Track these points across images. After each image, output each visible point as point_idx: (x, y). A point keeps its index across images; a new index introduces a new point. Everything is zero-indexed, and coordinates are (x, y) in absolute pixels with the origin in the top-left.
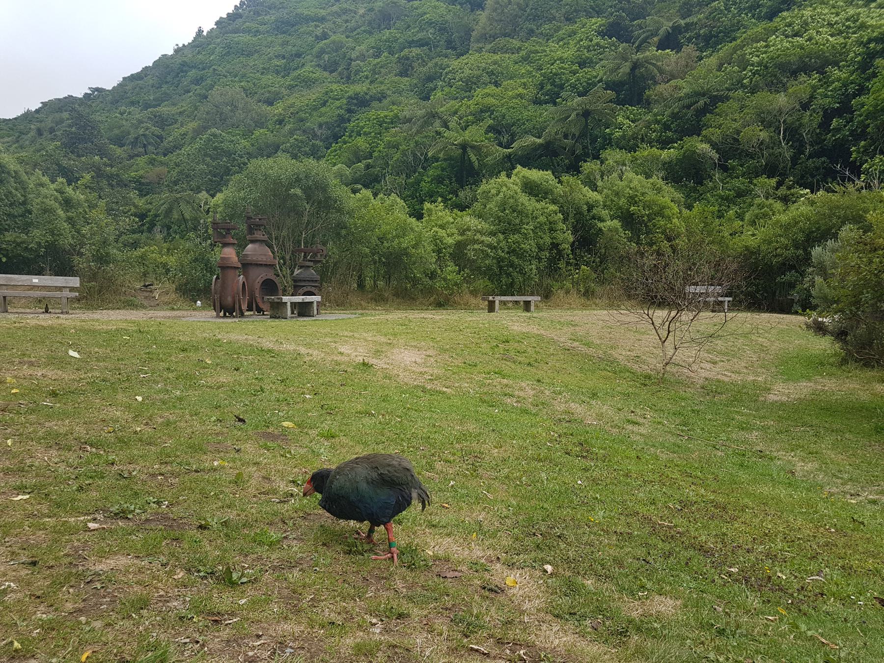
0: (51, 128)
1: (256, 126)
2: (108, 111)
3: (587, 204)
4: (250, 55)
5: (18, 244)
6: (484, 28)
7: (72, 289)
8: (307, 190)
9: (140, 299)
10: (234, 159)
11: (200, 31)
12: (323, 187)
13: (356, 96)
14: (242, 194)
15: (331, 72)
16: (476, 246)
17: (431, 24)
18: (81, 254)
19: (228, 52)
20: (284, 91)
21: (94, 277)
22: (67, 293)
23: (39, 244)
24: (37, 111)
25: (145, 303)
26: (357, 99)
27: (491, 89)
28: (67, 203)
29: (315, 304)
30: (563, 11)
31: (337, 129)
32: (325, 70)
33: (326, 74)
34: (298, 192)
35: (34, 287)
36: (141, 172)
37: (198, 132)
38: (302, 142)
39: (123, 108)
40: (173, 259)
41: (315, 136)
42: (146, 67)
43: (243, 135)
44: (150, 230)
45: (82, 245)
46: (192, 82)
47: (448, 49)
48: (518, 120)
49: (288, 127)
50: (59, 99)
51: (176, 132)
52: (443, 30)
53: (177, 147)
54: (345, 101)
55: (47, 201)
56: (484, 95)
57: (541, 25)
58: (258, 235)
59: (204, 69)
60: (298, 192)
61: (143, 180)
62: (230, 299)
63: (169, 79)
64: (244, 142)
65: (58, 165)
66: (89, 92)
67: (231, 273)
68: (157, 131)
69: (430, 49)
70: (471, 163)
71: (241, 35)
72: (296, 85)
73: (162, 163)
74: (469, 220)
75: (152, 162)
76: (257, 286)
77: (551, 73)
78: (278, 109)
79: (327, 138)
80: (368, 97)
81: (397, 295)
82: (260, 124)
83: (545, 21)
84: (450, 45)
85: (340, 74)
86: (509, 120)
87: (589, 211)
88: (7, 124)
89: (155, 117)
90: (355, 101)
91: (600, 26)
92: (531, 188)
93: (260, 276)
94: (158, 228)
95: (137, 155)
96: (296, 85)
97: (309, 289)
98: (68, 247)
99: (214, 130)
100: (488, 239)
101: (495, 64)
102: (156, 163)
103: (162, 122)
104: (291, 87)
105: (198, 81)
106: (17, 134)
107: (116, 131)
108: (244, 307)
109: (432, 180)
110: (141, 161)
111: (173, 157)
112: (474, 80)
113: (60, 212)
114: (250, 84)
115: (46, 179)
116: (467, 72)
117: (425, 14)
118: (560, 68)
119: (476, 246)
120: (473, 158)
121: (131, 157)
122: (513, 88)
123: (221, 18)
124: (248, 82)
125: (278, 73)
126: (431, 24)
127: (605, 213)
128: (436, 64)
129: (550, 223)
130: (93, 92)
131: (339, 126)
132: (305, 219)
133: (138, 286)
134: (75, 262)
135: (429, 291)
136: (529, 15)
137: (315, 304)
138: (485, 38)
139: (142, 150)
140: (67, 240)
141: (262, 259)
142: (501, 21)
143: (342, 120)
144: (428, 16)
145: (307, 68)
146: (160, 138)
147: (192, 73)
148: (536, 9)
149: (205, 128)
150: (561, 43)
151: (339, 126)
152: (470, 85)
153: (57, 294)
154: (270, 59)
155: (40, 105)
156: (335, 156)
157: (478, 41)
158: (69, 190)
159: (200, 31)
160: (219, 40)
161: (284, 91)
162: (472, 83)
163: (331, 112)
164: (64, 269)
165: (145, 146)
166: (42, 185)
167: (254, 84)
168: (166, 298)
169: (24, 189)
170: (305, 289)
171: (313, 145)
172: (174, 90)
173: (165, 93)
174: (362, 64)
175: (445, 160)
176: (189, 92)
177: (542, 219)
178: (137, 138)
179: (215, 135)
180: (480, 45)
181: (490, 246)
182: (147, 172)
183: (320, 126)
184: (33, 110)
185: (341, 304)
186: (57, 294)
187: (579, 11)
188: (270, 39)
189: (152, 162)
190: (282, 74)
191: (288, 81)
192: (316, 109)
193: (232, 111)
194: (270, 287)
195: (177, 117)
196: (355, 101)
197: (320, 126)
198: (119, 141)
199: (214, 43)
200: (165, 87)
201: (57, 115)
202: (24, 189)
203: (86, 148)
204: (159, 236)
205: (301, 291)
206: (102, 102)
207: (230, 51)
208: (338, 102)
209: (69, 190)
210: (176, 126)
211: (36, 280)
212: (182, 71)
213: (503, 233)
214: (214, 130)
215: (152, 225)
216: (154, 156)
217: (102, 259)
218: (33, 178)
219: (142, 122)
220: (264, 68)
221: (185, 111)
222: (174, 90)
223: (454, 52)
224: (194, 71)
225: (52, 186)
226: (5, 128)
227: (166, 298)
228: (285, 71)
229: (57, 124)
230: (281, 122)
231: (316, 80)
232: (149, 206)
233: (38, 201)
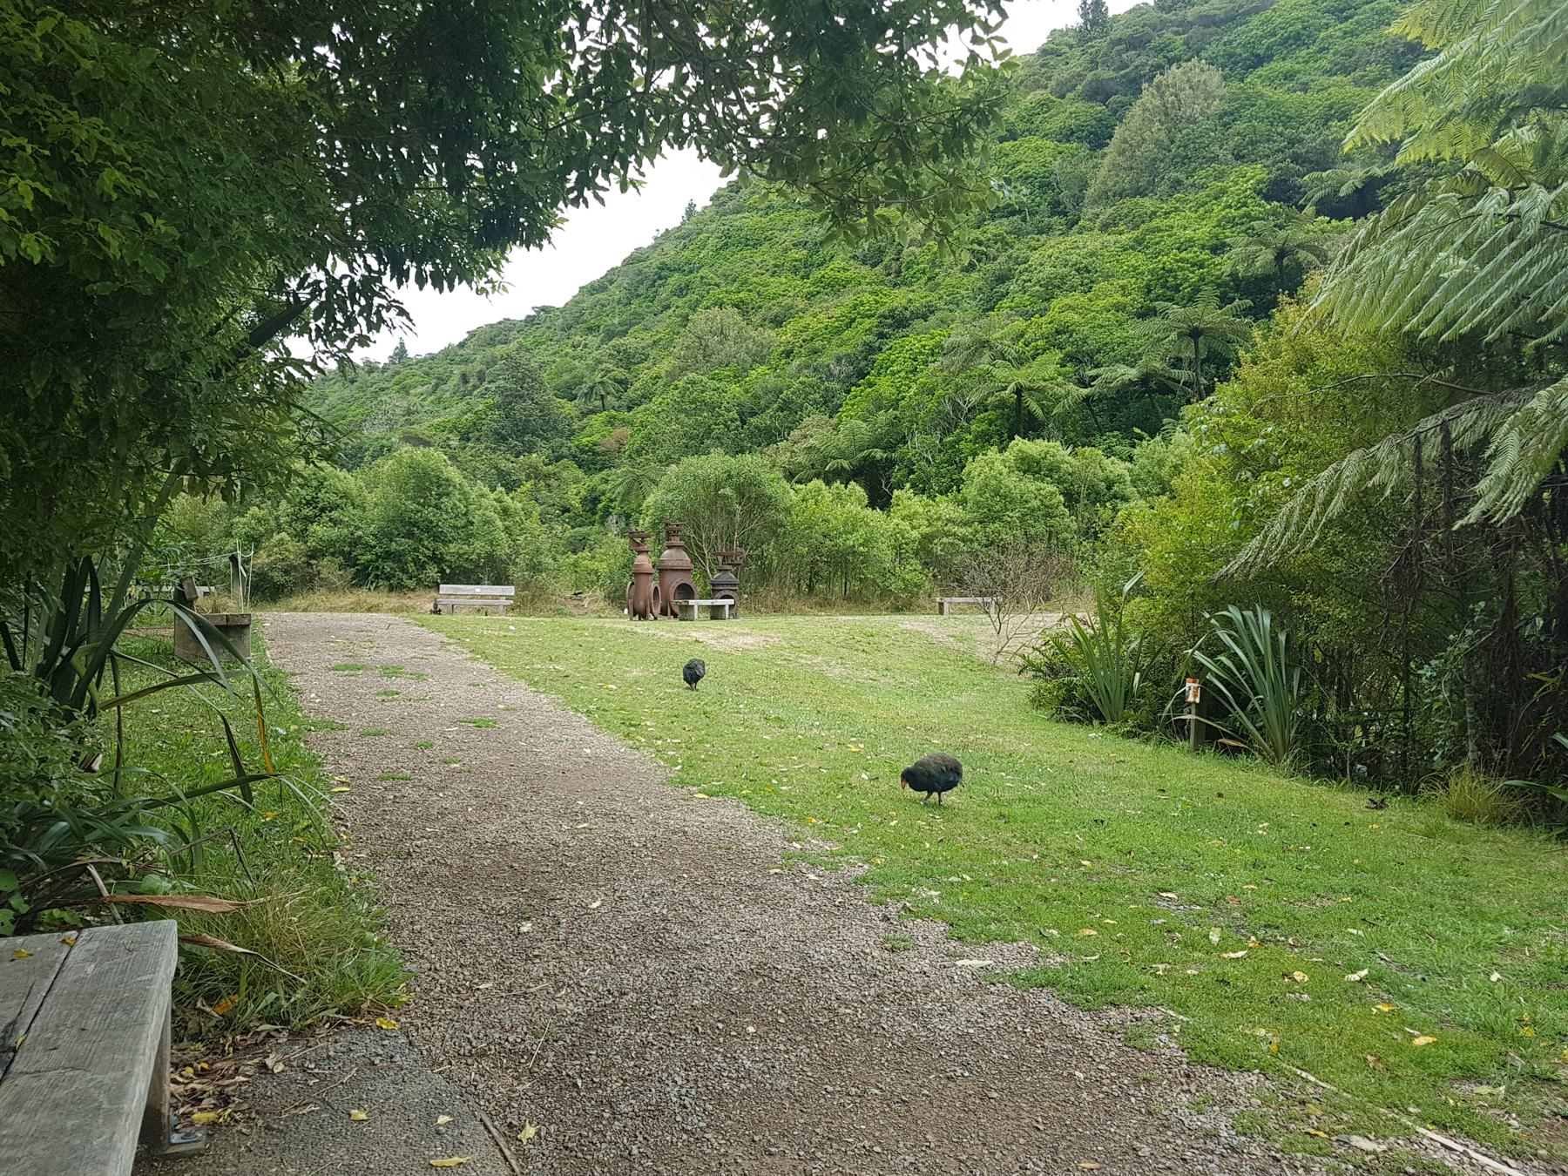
0: (480, 372)
1: (754, 361)
2: (558, 341)
3: (1106, 479)
4: (757, 244)
5: (460, 556)
6: (1104, 183)
7: (508, 598)
8: (740, 490)
9: (569, 608)
10: (720, 415)
11: (691, 206)
12: (753, 483)
13: (892, 314)
14: (670, 497)
15: (874, 265)
16: (945, 540)
17: (1027, 178)
18: (515, 564)
19: (726, 244)
20: (801, 303)
21: (526, 586)
22: (503, 601)
23: (479, 555)
24: (462, 345)
25: (574, 611)
26: (893, 317)
27: (1077, 298)
28: (505, 512)
29: (727, 608)
30: (1232, 144)
31: (863, 363)
32: (864, 263)
33: (865, 270)
34: (728, 491)
35: (474, 596)
36: (596, 437)
37: (673, 376)
38: (811, 386)
39: (578, 338)
40: (604, 565)
41: (830, 376)
42: (613, 269)
43: (735, 376)
44: (603, 521)
45: (518, 554)
46: (674, 293)
47: (1052, 215)
48: (1106, 344)
49: (796, 362)
50: (491, 326)
51: (644, 375)
52: (1045, 186)
53: (647, 397)
54: (875, 321)
55: (487, 512)
56: (1065, 307)
57: (1194, 169)
58: (676, 541)
59: (691, 272)
60: (728, 491)
61: (597, 449)
62: (642, 603)
63: (641, 290)
64: (735, 389)
65: (496, 468)
66: (533, 313)
67: (643, 579)
68: (620, 373)
69: (1024, 220)
70: (1031, 414)
71: (746, 214)
72: (818, 292)
73: (625, 422)
74: (945, 507)
75: (611, 422)
76: (672, 590)
77: (1163, 269)
78: (786, 335)
79: (848, 377)
80: (908, 314)
81: (847, 599)
82: (759, 358)
83: (1201, 164)
84: (1056, 208)
85: (886, 267)
86: (1092, 345)
87: (1109, 488)
88: (421, 367)
89: (619, 352)
90: (889, 321)
91: (1259, 182)
92: (1029, 466)
93: (675, 581)
94: (612, 519)
95: (593, 412)
96: (818, 292)
97: (727, 593)
98: (504, 557)
99: (691, 375)
100: (962, 531)
101: (1091, 256)
102: (617, 423)
103: (628, 359)
104: (810, 296)
105: (681, 291)
106: (434, 382)
107: (566, 377)
108: (657, 611)
109: (976, 437)
110: (597, 420)
111: (638, 414)
112: (1056, 282)
113: (499, 523)
114: (754, 295)
115: (486, 490)
116: (1048, 270)
117: (1018, 162)
118: (1177, 261)
119: (945, 540)
120: (1034, 406)
121: (584, 415)
122: (1108, 294)
123: (720, 189)
124: (750, 291)
125: (795, 271)
126: (1027, 178)
127: (1130, 490)
128: (1010, 257)
129: (1046, 507)
130: (538, 313)
131: (865, 359)
132: (738, 518)
133: (569, 594)
134: (511, 572)
135: (885, 593)
136: (1175, 157)
137: (727, 608)
138: (1105, 197)
139: (598, 403)
140: (503, 551)
141: (679, 565)
142: (1132, 169)
143: (871, 349)
144: (1021, 166)
145: (838, 263)
146: (624, 383)
147: (675, 279)
148: (1186, 146)
149: (683, 370)
150: (1201, 210)
151: (865, 359)
152: (1050, 290)
153: (496, 602)
154: (786, 250)
155: (466, 336)
156: (853, 405)
157: (1095, 202)
158: (507, 499)
159: (691, 206)
160: (714, 225)
161: (801, 303)
162: (1055, 287)
163: (857, 337)
164: (500, 580)
165: (602, 397)
166: (482, 496)
167: (758, 293)
168: (594, 607)
169: (466, 499)
170: (723, 593)
171: (826, 390)
172: (648, 307)
173: (635, 313)
174: (917, 251)
175: (995, 408)
176: (668, 307)
177: (1035, 503)
178: (592, 388)
179: (693, 383)
180: (1097, 210)
181: (964, 540)
182: (604, 436)
183: (839, 360)
184: (456, 343)
185: (754, 610)
186: (496, 602)
187: (1257, 142)
188: (787, 218)
189: (611, 422)
190: (802, 273)
191: (808, 286)
192: (838, 331)
193: (721, 342)
194: (686, 591)
195: (648, 350)
196: (889, 321)
197: (839, 360)
198: (569, 393)
199: (707, 231)
200: (636, 302)
201: (489, 351)
202: (466, 499)
203: (525, 410)
204: (614, 529)
205: (718, 595)
206: (549, 328)
207: (729, 241)
208: (868, 321)
209: (507, 499)
210: (646, 364)
211: (478, 589)
212: (660, 278)
213: (980, 523)
214: (691, 375)
215: (607, 513)
216: (614, 413)
217: (535, 568)
218: (476, 489)
219: (601, 363)
220: (776, 266)
221: (660, 339)
222: (648, 307)
223: (1063, 221)
224: (676, 275)
225: (493, 496)
226: (418, 372)
227: (594, 607)
228: (803, 269)
229: (488, 365)
230: (788, 354)
231: (848, 282)
232: (602, 487)
233: (480, 512)
